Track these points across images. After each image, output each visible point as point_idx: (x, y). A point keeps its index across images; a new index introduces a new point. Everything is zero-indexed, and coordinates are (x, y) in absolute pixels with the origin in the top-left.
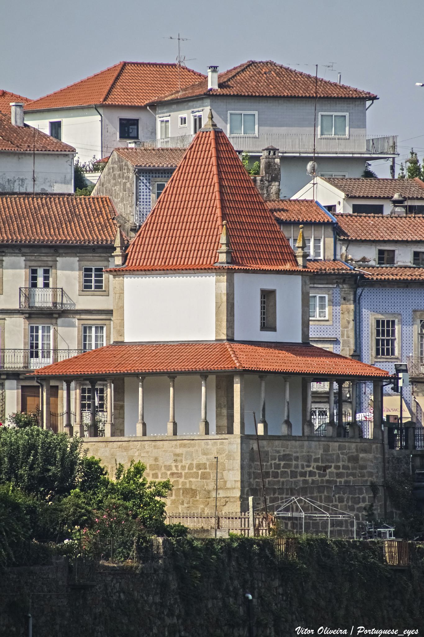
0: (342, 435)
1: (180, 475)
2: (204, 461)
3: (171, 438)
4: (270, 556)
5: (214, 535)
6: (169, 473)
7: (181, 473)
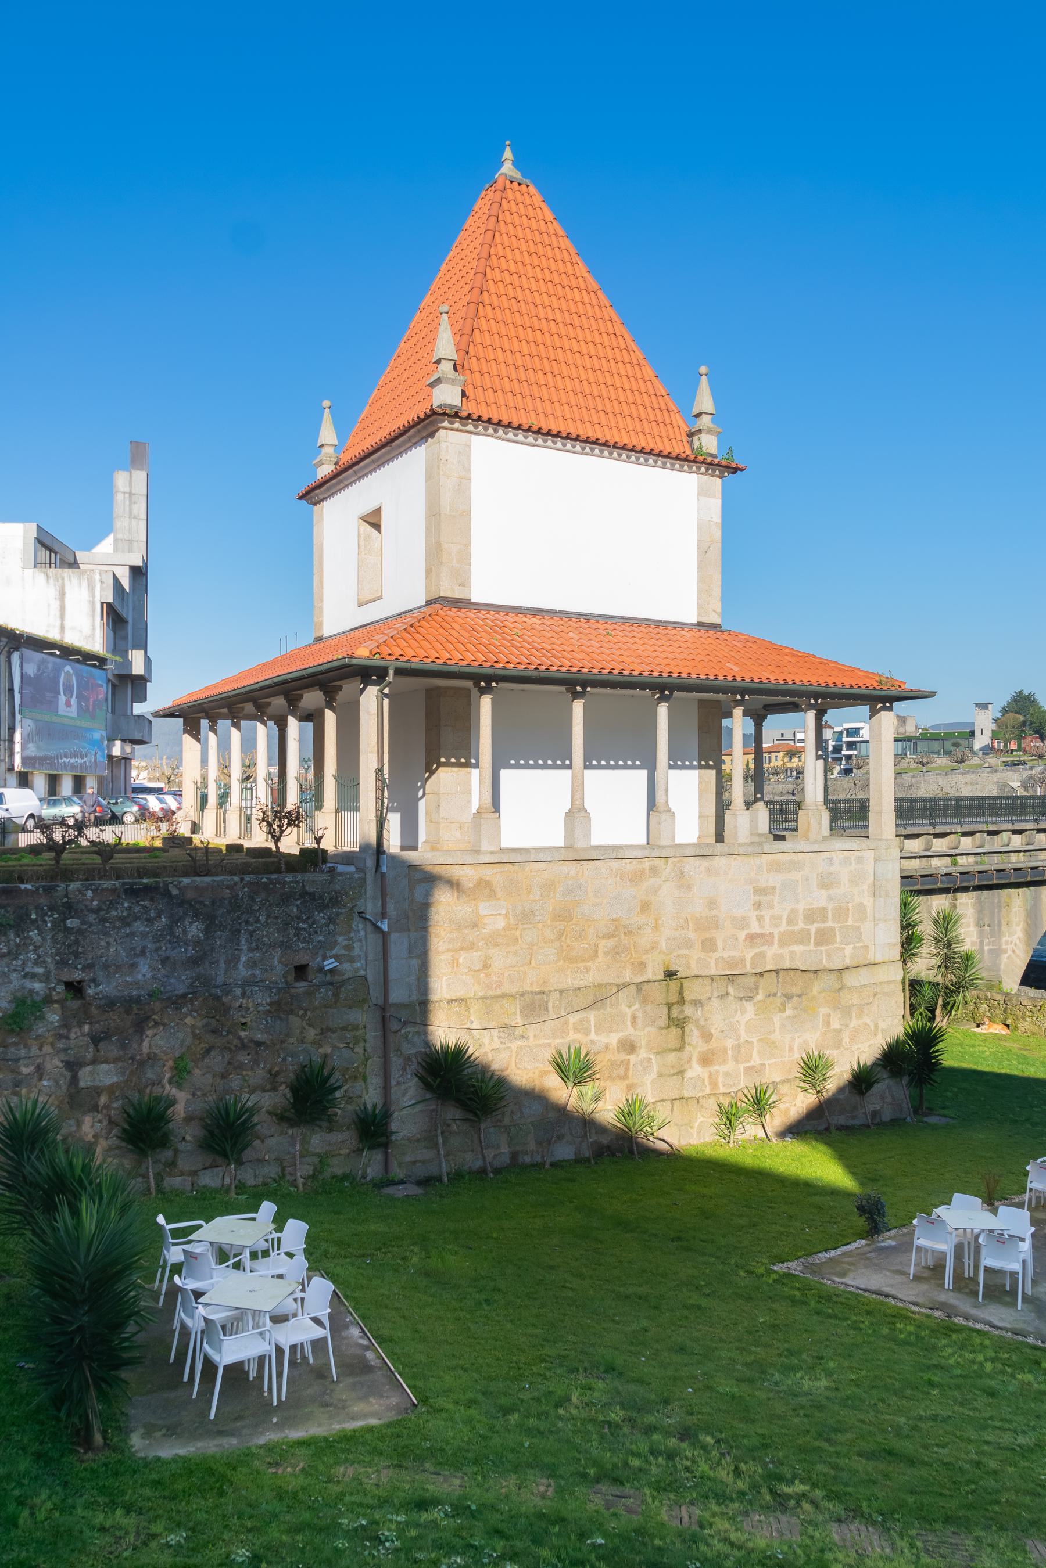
0: (930, 786)
1: (764, 938)
2: (823, 903)
6: (742, 935)
7: (771, 934)
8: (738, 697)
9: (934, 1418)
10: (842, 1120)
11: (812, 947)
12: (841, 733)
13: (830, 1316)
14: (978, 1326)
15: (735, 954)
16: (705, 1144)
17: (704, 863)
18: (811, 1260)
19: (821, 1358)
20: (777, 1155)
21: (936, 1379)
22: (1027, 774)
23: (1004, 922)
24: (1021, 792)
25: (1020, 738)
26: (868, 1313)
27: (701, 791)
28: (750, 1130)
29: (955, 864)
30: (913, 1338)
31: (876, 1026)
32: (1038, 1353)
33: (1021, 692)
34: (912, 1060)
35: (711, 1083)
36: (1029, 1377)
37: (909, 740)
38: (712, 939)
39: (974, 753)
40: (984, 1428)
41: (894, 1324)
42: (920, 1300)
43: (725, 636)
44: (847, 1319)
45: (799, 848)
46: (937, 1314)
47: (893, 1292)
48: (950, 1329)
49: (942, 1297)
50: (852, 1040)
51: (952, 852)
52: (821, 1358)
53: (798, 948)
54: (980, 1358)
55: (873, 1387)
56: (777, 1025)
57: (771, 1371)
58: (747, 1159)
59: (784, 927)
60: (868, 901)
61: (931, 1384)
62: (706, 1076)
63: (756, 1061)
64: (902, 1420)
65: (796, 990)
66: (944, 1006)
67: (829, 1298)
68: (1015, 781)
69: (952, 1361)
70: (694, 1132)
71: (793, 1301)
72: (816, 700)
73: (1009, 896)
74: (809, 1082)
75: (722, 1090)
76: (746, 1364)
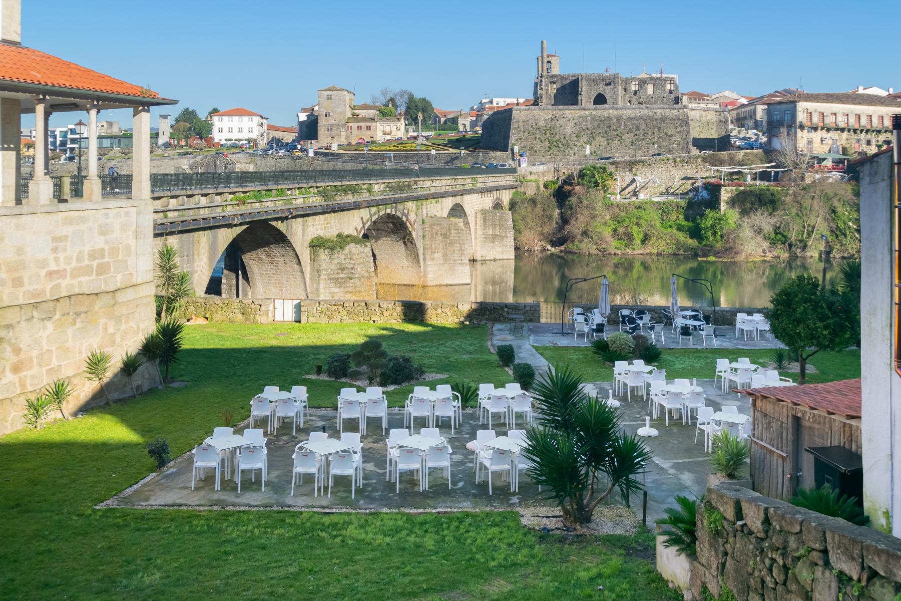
1: (61, 273)
2: (102, 245)
3: (49, 209)
4: (307, 377)
5: (758, 317)
6: (43, 273)
7: (65, 270)
8: (41, 96)
9: (236, 574)
10: (116, 396)
11: (94, 277)
12: (66, 132)
13: (147, 530)
14: (242, 508)
15: (39, 287)
16: (18, 432)
17: (14, 220)
18: (121, 496)
19: (150, 559)
20: (76, 429)
21: (228, 549)
22: (193, 160)
23: (196, 253)
24: (188, 171)
25: (187, 138)
26: (172, 520)
27: (3, 167)
28: (52, 414)
29: (166, 217)
30: (205, 528)
31: (138, 327)
32: (281, 515)
33: (187, 109)
34: (163, 348)
35: (20, 386)
36: (282, 531)
37: (115, 137)
38: (20, 277)
39: (159, 147)
40: (267, 570)
41: (190, 522)
42: (202, 502)
43: (25, 51)
44: (158, 528)
45: (85, 206)
46: (215, 508)
47: (184, 502)
48: (226, 516)
49: (216, 497)
50: (122, 339)
51: (165, 209)
52: (150, 559)
53: (84, 279)
54: (250, 528)
55: (192, 567)
56: (70, 335)
57: (119, 579)
58: (55, 435)
59: (74, 264)
60: (132, 242)
61: (226, 553)
62: (17, 380)
63: (55, 363)
64: (218, 582)
65: (83, 309)
66: (167, 310)
67: (142, 518)
68: (185, 165)
69: (234, 535)
70: (8, 425)
71: (118, 527)
72: (98, 102)
73: (199, 236)
74: (94, 373)
75: (29, 389)
76: (99, 581)
